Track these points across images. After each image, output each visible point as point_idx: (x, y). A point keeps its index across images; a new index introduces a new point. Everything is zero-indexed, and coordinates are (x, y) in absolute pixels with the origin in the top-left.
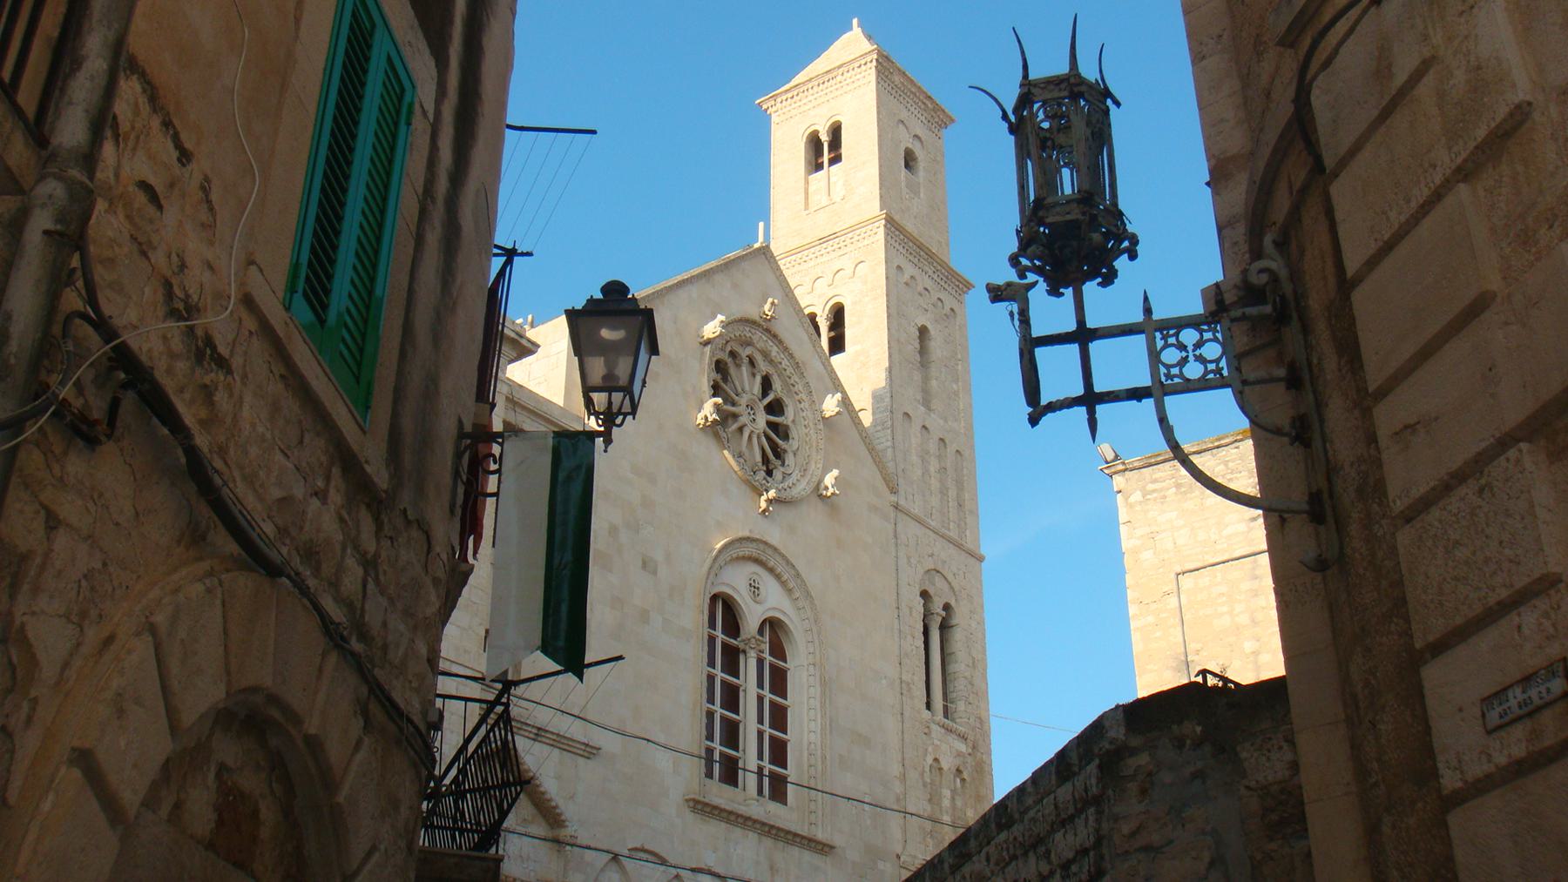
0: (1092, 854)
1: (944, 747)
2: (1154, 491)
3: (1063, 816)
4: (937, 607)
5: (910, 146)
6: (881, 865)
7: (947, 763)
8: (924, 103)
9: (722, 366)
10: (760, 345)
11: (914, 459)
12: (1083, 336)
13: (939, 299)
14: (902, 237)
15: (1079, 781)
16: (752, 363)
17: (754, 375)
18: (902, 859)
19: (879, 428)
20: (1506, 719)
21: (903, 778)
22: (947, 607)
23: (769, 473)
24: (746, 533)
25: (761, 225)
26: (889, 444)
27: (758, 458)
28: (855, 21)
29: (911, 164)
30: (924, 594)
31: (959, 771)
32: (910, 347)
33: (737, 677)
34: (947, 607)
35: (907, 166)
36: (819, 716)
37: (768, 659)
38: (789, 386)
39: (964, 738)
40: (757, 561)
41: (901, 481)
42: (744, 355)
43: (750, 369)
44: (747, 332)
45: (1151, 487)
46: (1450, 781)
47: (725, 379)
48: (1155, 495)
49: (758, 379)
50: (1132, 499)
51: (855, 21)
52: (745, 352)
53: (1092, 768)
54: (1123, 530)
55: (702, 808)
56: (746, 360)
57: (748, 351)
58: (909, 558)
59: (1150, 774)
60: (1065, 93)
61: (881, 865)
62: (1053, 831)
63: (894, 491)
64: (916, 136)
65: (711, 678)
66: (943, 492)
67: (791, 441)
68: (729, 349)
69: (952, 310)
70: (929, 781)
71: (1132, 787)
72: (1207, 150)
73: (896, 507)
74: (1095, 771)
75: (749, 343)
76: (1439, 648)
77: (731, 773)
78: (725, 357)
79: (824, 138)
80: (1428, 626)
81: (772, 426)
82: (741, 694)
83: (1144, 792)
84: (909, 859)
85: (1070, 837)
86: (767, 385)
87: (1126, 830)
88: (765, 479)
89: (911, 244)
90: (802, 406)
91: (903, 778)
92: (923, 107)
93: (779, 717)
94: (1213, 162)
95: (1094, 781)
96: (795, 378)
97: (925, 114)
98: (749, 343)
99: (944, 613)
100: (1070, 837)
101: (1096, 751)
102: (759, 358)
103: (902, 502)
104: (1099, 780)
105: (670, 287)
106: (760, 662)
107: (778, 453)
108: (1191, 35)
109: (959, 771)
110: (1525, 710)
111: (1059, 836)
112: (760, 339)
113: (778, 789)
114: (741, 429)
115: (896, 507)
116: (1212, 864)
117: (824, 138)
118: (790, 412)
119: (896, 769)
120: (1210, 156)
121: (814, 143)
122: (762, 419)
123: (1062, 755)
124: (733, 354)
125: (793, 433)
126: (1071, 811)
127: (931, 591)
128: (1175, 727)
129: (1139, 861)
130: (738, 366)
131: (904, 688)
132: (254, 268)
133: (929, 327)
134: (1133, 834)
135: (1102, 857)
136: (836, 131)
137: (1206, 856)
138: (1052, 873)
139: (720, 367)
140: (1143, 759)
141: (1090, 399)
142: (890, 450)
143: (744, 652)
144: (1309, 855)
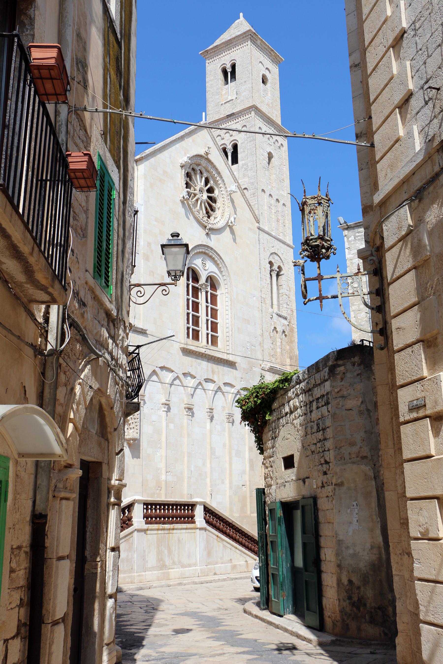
0: (326, 397)
1: (278, 322)
2: (359, 236)
3: (317, 383)
4: (275, 267)
5: (265, 73)
6: (254, 369)
7: (279, 329)
8: (270, 53)
9: (189, 174)
10: (204, 165)
11: (266, 207)
12: (320, 278)
13: (276, 140)
14: (261, 114)
15: (322, 373)
16: (201, 173)
17: (202, 177)
18: (262, 366)
19: (252, 196)
20: (413, 408)
21: (262, 335)
22: (279, 267)
23: (209, 217)
24: (201, 243)
25: (204, 113)
26: (256, 202)
27: (205, 212)
28: (241, 14)
29: (265, 81)
30: (271, 263)
31: (284, 332)
32: (265, 162)
33: (198, 299)
34: (279, 267)
35: (263, 82)
36: (230, 313)
37: (210, 291)
38: (216, 182)
39: (285, 318)
40: (205, 253)
41: (261, 217)
42: (198, 170)
43: (200, 175)
44: (198, 160)
45: (357, 234)
46: (402, 419)
47: (191, 180)
48: (359, 237)
49: (204, 179)
50: (350, 239)
51: (241, 14)
52: (197, 168)
53: (327, 369)
54: (347, 251)
55: (187, 352)
56: (199, 172)
57: (199, 168)
58: (264, 248)
59: (344, 373)
60: (317, 202)
61: (254, 369)
62: (314, 387)
63: (258, 222)
64: (267, 68)
65: (188, 300)
66: (278, 221)
67: (217, 204)
68: (191, 167)
69: (281, 144)
70: (272, 336)
71: (339, 377)
72: (362, 202)
73: (259, 228)
74: (327, 370)
75: (198, 165)
76: (402, 386)
77: (196, 336)
78: (190, 171)
79: (229, 70)
80: (400, 381)
81: (210, 198)
82: (200, 306)
83: (342, 379)
84: (264, 366)
85: (319, 390)
86: (207, 181)
87: (336, 390)
88: (207, 220)
89: (265, 117)
90: (221, 189)
91: (262, 335)
92: (270, 55)
93: (214, 313)
94: (363, 206)
95: (327, 374)
96: (218, 178)
97: (271, 58)
98: (198, 165)
99: (278, 270)
100: (319, 390)
101: (328, 364)
102: (203, 170)
103: (262, 226)
104: (328, 374)
105: (168, 144)
106: (207, 292)
107: (213, 210)
108: (359, 160)
109: (284, 332)
110: (416, 407)
111: (316, 389)
112: (203, 163)
113: (214, 341)
114: (197, 200)
115: (259, 228)
116: (362, 402)
117: (213, 204)
118: (216, 192)
119: (259, 332)
120: (362, 205)
121: (225, 72)
122: (205, 196)
123: (317, 363)
124: (193, 169)
125: (218, 201)
126: (319, 382)
127: (273, 261)
128: (352, 359)
129: (340, 400)
130: (195, 174)
131: (263, 301)
132: (87, 273)
133: (272, 152)
134: (338, 392)
135: (329, 398)
136: (233, 66)
137: (361, 400)
138: (313, 401)
139: (188, 175)
140: (342, 368)
141: (321, 298)
142: (257, 205)
143: (201, 289)
144: (378, 419)
